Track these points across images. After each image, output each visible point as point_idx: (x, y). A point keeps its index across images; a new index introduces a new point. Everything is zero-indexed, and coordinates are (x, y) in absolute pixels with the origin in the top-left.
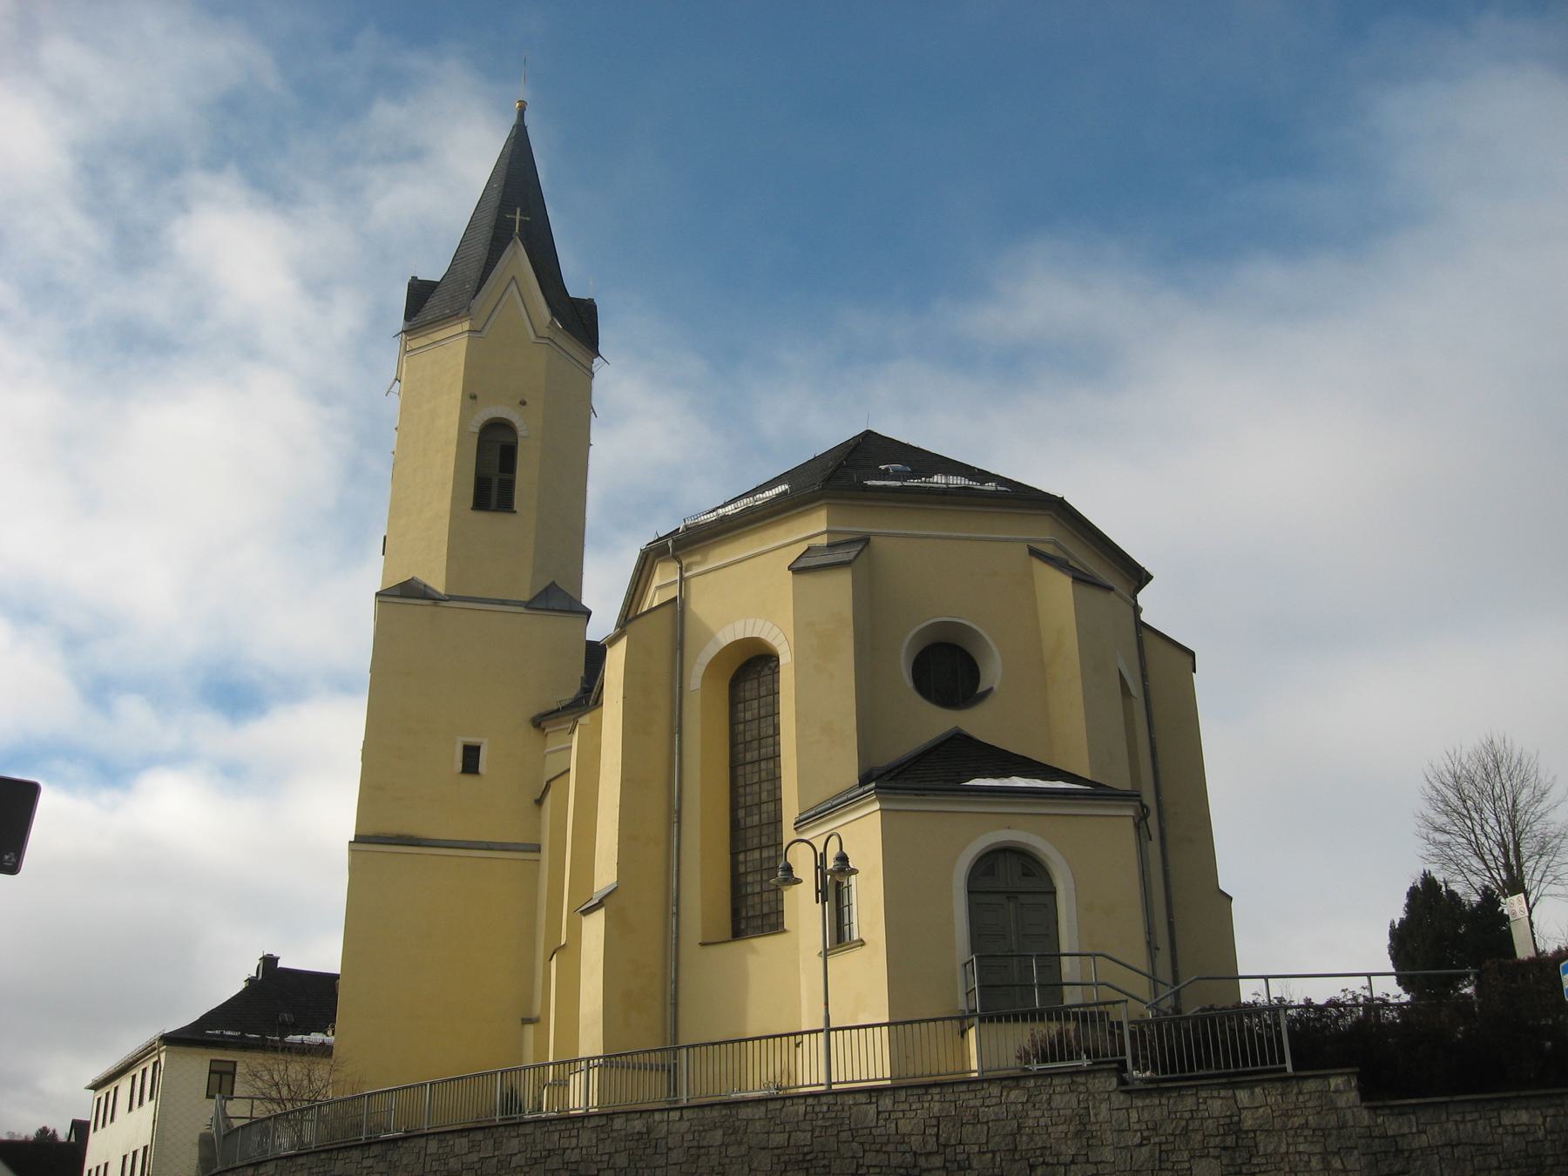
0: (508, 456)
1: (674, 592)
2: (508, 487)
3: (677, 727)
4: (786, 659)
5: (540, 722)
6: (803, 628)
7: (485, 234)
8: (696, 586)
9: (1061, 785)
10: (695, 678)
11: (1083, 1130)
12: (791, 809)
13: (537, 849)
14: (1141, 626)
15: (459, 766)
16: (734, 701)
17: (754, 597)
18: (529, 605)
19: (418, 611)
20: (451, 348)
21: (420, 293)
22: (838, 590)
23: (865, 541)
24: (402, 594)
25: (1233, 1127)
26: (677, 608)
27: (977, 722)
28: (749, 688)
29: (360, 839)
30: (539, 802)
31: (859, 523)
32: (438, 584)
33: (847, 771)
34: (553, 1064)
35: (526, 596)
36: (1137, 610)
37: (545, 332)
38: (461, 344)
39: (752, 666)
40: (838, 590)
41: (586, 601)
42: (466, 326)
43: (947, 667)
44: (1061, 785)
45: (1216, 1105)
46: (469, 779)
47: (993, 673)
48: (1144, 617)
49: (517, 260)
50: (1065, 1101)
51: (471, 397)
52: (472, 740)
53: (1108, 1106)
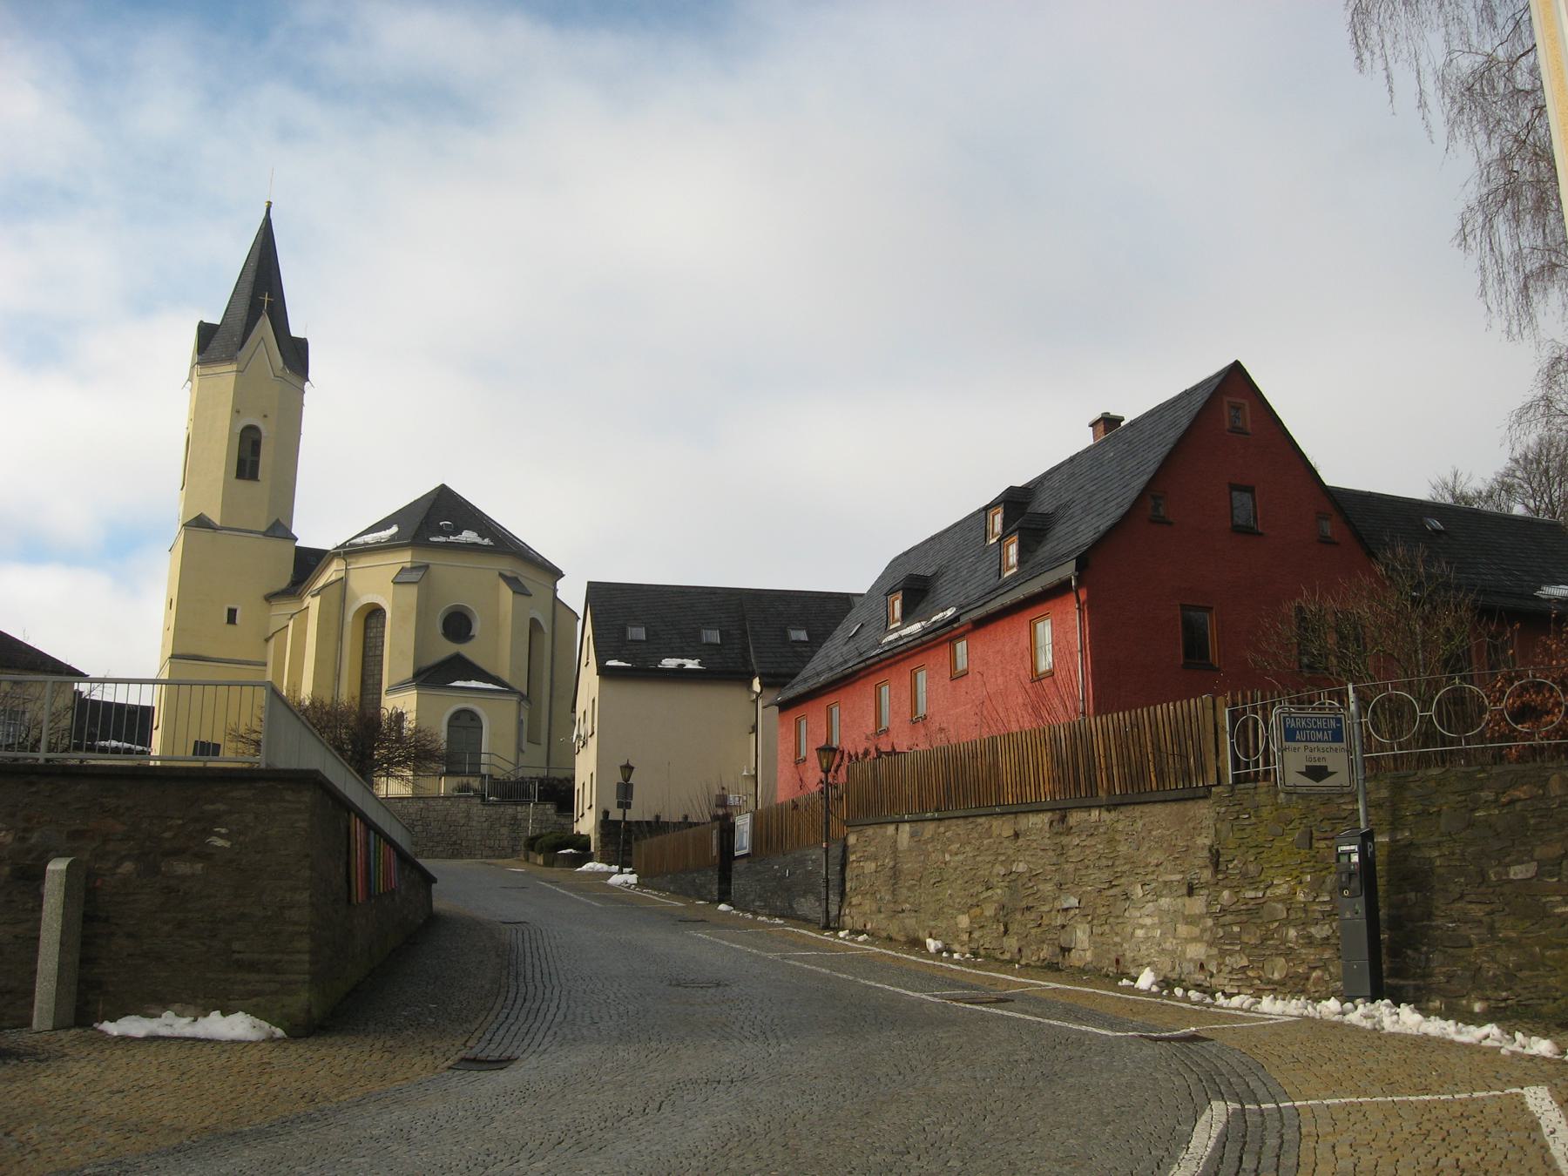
0: (256, 446)
1: (342, 574)
2: (255, 464)
3: (341, 638)
4: (388, 615)
5: (271, 598)
6: (395, 607)
7: (243, 305)
8: (352, 574)
9: (490, 686)
10: (349, 617)
11: (468, 816)
12: (385, 686)
13: (265, 665)
14: (555, 597)
15: (225, 619)
16: (366, 628)
17: (374, 583)
18: (265, 534)
19: (205, 534)
20: (226, 376)
21: (206, 333)
22: (411, 594)
23: (427, 567)
24: (198, 523)
25: (514, 818)
26: (343, 583)
27: (467, 650)
28: (373, 622)
29: (173, 657)
30: (267, 640)
31: (426, 558)
32: (216, 519)
33: (408, 673)
34: (1243, 1109)
35: (263, 529)
36: (555, 590)
37: (279, 373)
38: (232, 378)
39: (374, 614)
40: (411, 594)
41: (1084, 439)
42: (234, 367)
43: (458, 625)
44: (490, 686)
45: (510, 810)
46: (231, 627)
47: (477, 629)
48: (559, 595)
49: (265, 326)
50: (463, 806)
51: (236, 412)
52: (233, 606)
53: (477, 809)
